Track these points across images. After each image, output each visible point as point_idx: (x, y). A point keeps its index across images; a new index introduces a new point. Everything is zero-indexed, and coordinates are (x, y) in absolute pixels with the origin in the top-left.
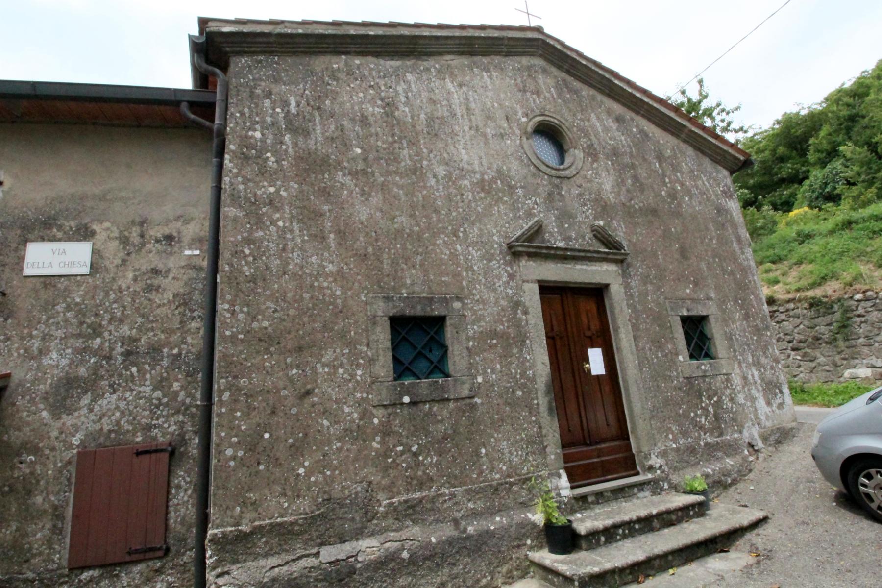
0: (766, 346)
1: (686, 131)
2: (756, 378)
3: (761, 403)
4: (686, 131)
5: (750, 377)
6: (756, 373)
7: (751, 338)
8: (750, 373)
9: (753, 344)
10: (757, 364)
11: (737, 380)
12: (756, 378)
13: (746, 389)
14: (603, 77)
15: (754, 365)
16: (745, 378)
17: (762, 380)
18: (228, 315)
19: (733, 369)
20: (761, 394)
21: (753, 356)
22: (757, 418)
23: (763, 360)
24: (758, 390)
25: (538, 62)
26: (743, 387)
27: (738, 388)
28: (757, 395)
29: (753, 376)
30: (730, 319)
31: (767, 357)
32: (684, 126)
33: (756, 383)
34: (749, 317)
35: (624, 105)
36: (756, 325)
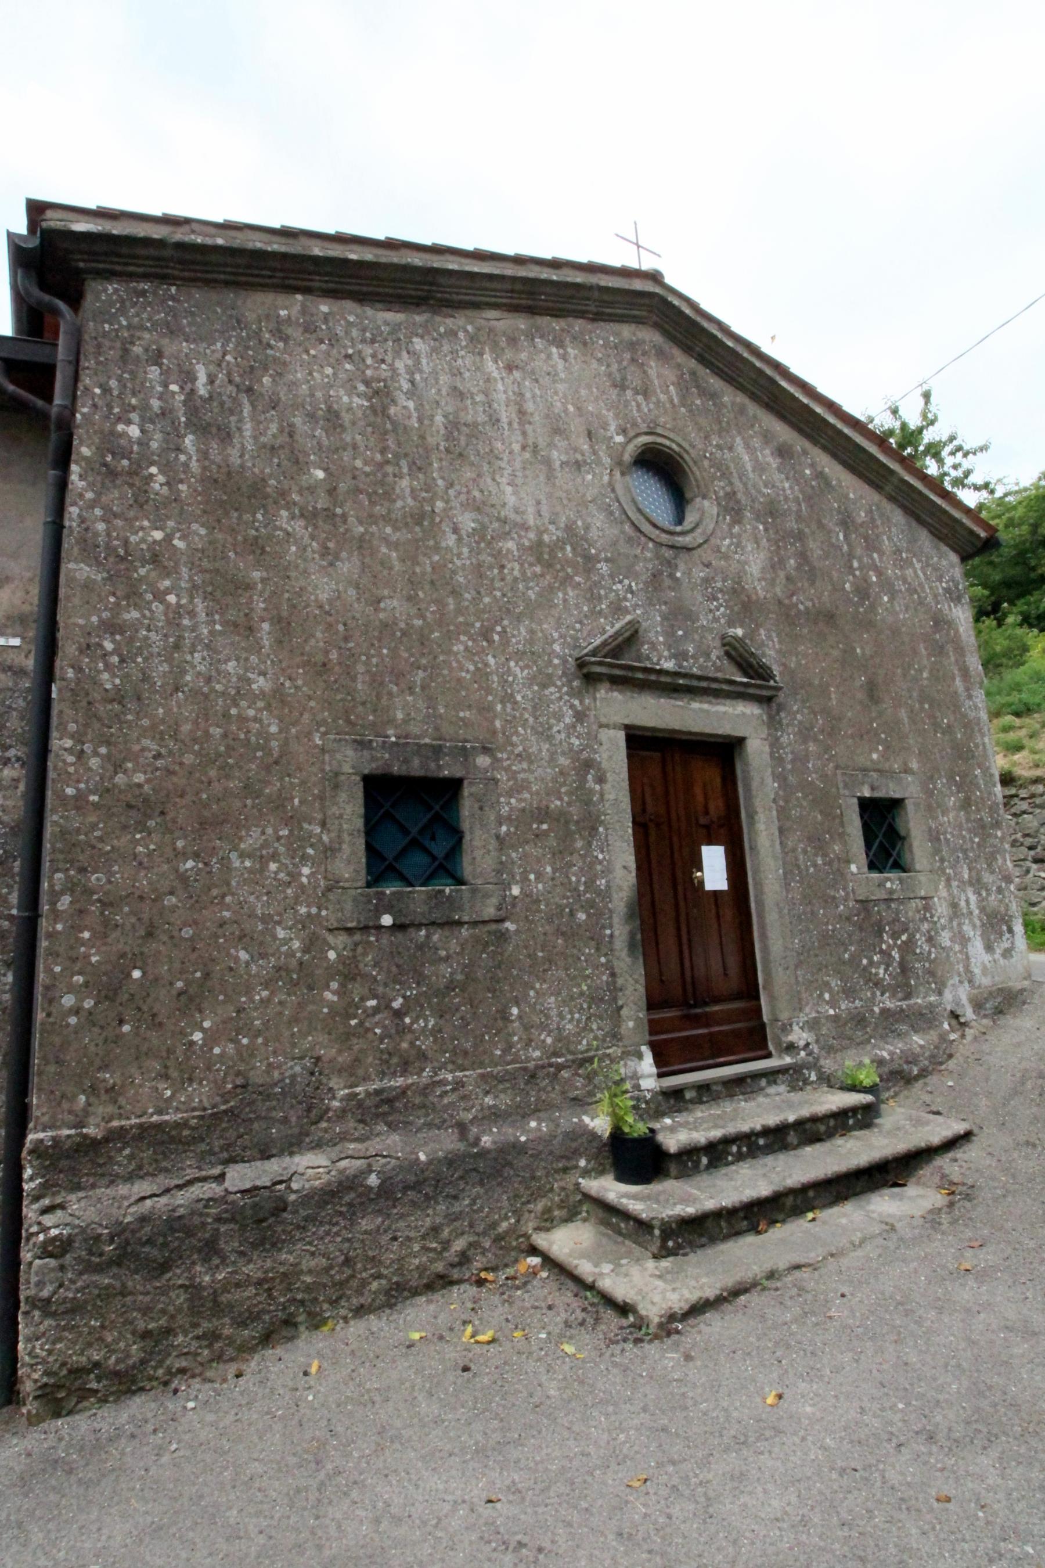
2: (973, 906)
6: (973, 898)
8: (963, 898)
10: (977, 883)
11: (941, 909)
12: (973, 906)
13: (955, 923)
16: (954, 905)
17: (982, 909)
21: (970, 870)
23: (987, 878)
26: (951, 920)
29: (967, 902)
30: (939, 806)
31: (993, 872)
34: (970, 806)
36: (981, 819)
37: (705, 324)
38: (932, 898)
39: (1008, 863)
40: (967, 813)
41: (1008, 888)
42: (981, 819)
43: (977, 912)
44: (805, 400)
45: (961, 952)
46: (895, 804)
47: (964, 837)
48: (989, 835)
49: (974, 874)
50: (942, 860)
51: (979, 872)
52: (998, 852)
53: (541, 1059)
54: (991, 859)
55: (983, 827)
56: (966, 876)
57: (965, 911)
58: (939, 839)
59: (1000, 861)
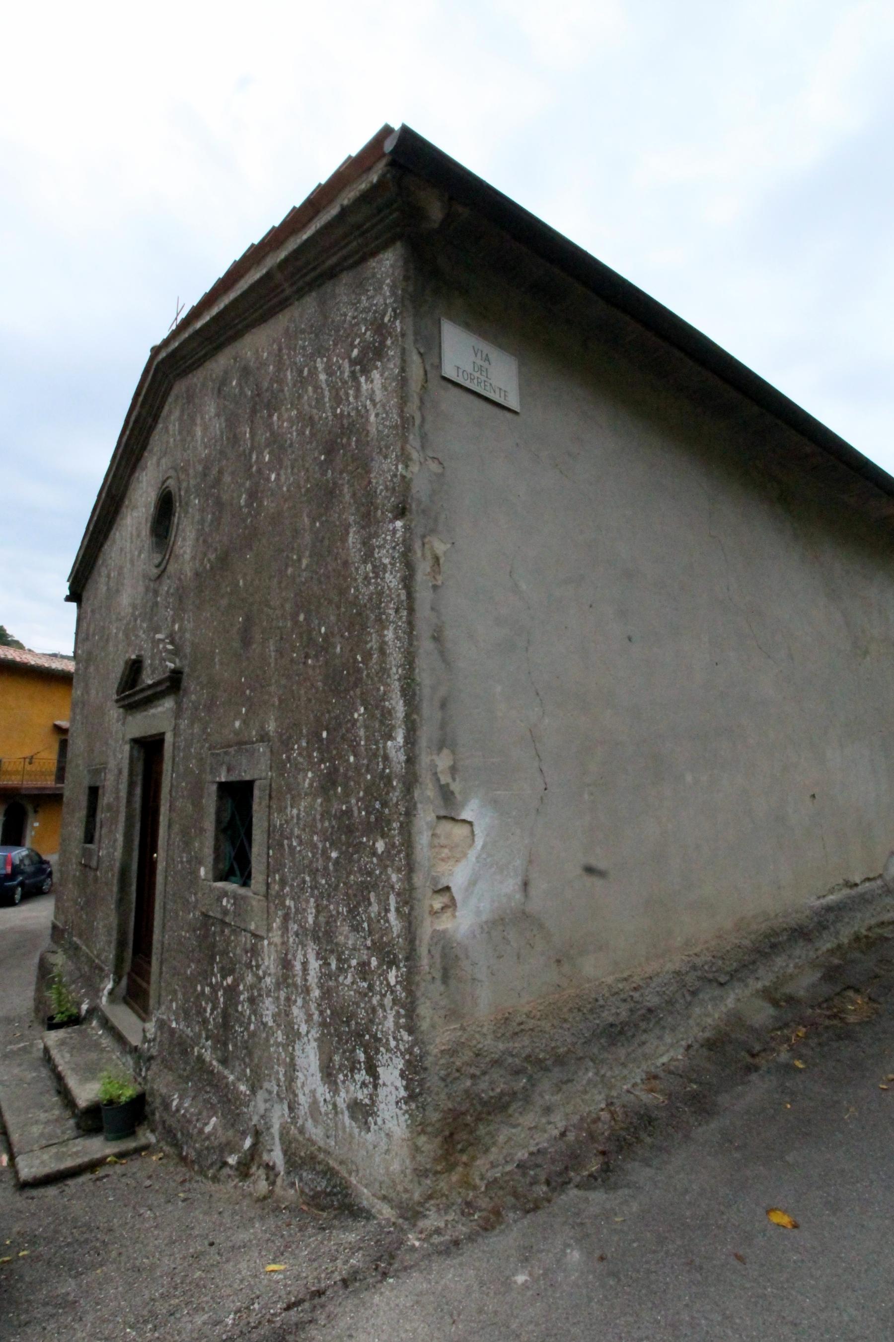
0: (365, 887)
1: (279, 276)
2: (313, 979)
3: (309, 1057)
4: (279, 276)
5: (298, 967)
6: (314, 965)
7: (324, 852)
8: (300, 957)
9: (326, 873)
10: (324, 936)
11: (269, 961)
12: (313, 979)
13: (282, 995)
14: (365, 198)
15: (316, 939)
16: (286, 964)
17: (327, 993)
18: (142, 1211)
19: (269, 929)
20: (315, 1033)
21: (319, 909)
22: (290, 1089)
23: (345, 936)
24: (309, 1018)
25: (180, 387)
26: (278, 986)
27: (268, 980)
28: (303, 1029)
29: (305, 964)
30: (290, 790)
31: (356, 928)
32: (268, 276)
33: (307, 990)
34: (334, 784)
35: (264, 318)
36: (348, 813)
37: (91, 529)
38: (262, 938)
39: (392, 916)
40: (327, 800)
41: (384, 974)
42: (348, 813)
43: (316, 993)
44: (334, 211)
45: (285, 1046)
46: (248, 786)
47: (315, 846)
48: (359, 847)
49: (322, 919)
50: (283, 882)
51: (331, 921)
52: (375, 886)
53: (375, 516)
54: (358, 897)
55: (350, 830)
56: (311, 920)
57: (299, 980)
58: (281, 845)
59: (375, 908)
